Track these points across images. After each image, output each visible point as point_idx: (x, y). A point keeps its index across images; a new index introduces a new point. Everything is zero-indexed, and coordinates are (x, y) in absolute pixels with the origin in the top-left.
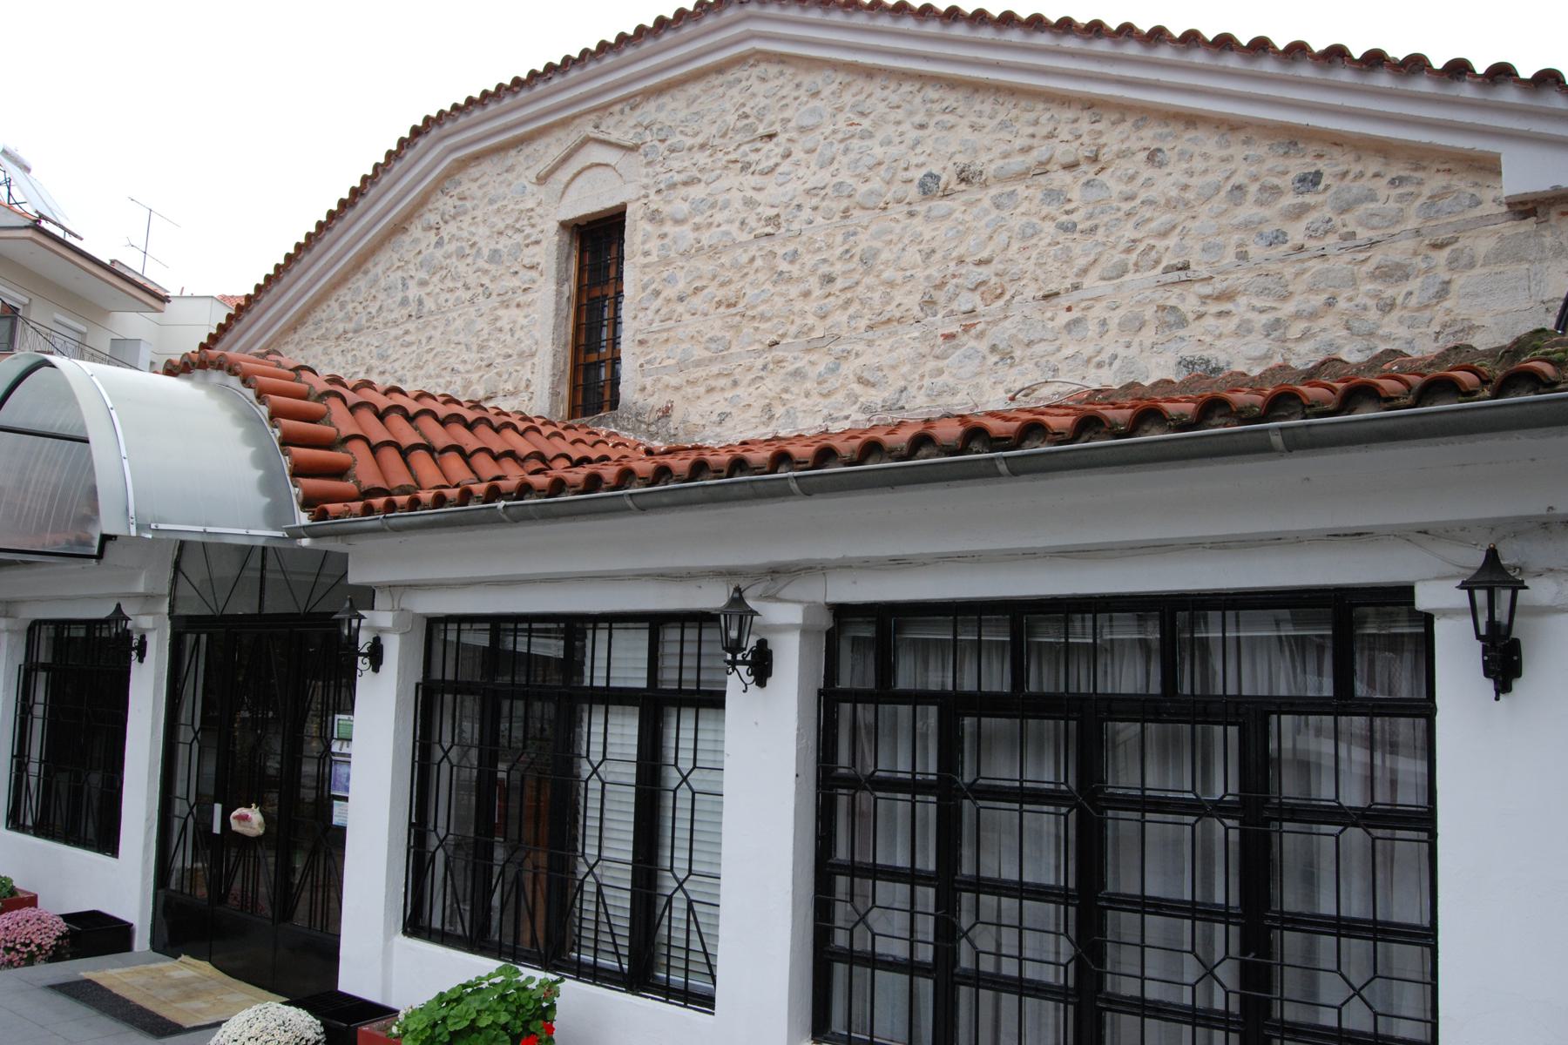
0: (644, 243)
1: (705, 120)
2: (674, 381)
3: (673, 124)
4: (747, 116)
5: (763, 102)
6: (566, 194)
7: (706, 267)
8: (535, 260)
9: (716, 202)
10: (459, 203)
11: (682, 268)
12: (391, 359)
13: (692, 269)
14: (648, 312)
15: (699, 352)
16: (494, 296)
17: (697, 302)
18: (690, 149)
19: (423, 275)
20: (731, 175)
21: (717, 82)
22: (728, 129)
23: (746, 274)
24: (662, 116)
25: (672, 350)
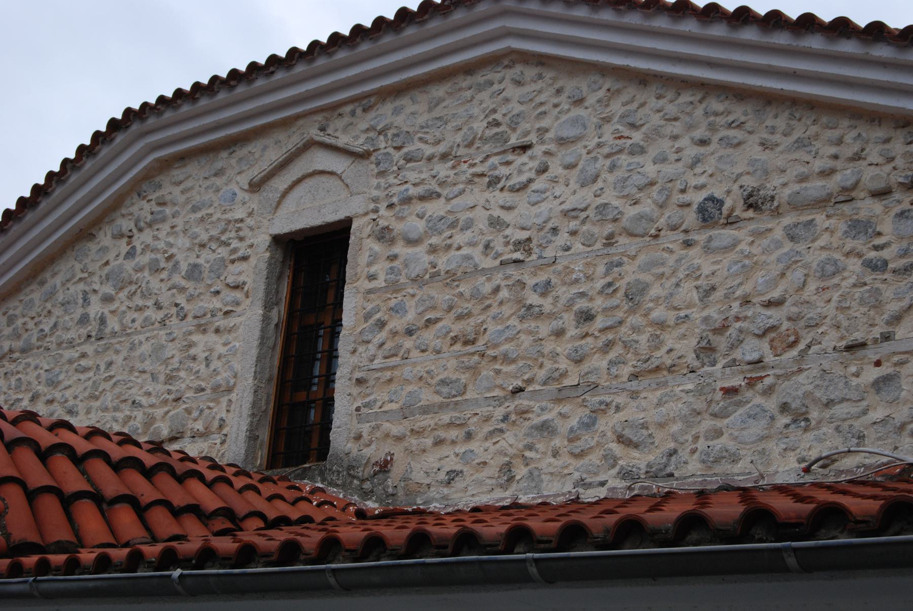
0: (369, 264)
4: (497, 124)
5: (517, 108)
6: (281, 206)
7: (442, 296)
8: (242, 279)
10: (157, 209)
11: (413, 296)
12: (62, 386)
13: (425, 297)
14: (370, 346)
15: (427, 397)
16: (189, 318)
17: (428, 336)
18: (430, 159)
20: (476, 190)
21: (464, 84)
22: (474, 138)
23: (489, 306)
24: (399, 120)
25: (395, 392)
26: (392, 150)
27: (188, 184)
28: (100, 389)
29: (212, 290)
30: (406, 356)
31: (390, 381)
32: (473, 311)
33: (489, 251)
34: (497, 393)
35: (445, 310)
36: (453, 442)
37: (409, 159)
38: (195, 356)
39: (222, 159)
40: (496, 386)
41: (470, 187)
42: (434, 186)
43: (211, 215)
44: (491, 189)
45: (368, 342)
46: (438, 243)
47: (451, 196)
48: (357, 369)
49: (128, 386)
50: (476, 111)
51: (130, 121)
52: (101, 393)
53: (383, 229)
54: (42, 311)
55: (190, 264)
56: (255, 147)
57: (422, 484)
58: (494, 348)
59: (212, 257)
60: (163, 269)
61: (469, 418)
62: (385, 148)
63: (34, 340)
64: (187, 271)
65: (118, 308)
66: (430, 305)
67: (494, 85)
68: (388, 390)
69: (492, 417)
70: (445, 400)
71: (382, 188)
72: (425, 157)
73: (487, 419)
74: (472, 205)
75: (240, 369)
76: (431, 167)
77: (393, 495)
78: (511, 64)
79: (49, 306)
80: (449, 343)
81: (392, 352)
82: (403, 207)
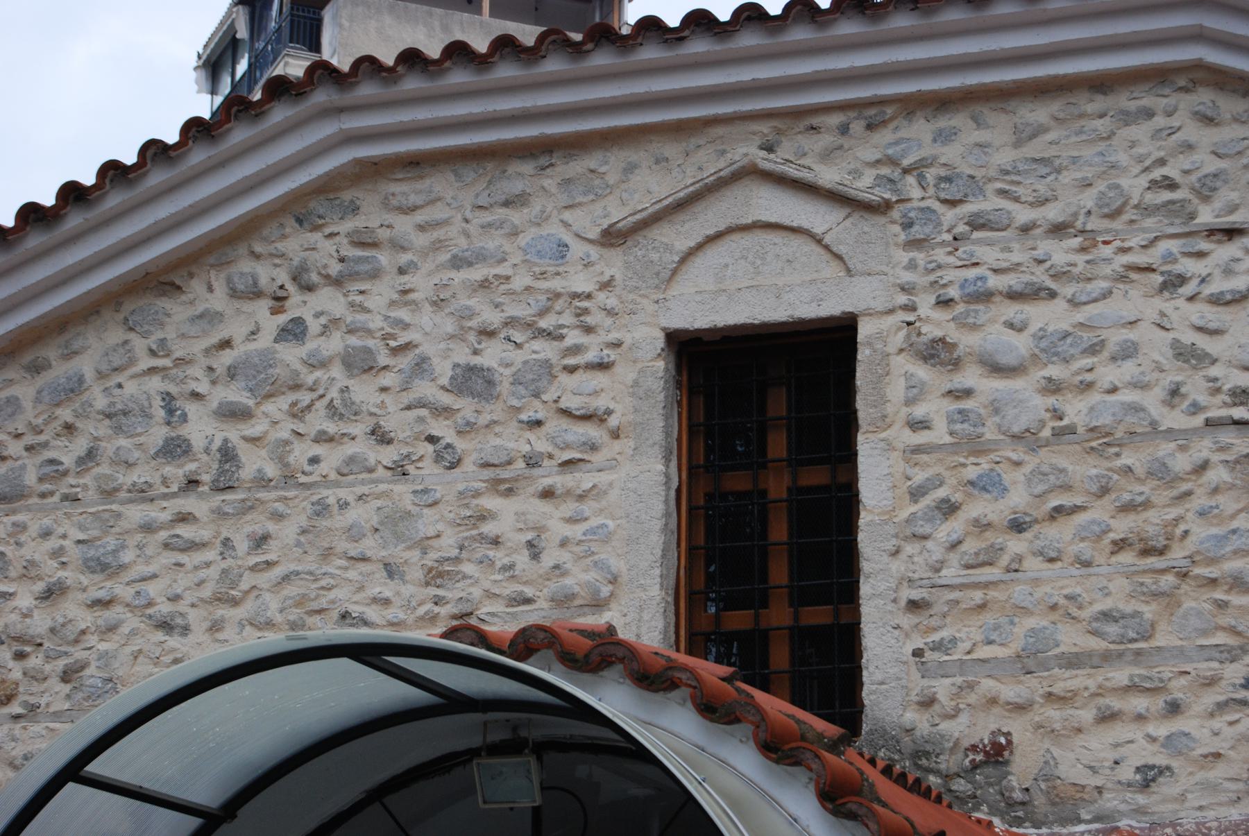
0: (909, 402)
1: (1066, 178)
2: (1009, 692)
3: (979, 174)
4: (1172, 186)
5: (1213, 165)
6: (678, 278)
7: (1084, 470)
8: (601, 403)
9: (1102, 343)
10: (352, 252)
11: (1018, 464)
12: (134, 573)
13: (1045, 468)
14: (929, 544)
15: (1071, 638)
16: (468, 466)
17: (1060, 534)
18: (1026, 229)
19: (235, 394)
20: (1133, 293)
21: (1090, 108)
22: (1125, 204)
23: (1188, 494)
24: (950, 153)
25: (996, 627)
26: (938, 203)
27: (437, 212)
28: (244, 586)
29: (524, 417)
30: (1015, 566)
31: (982, 607)
32: (1153, 499)
33: (1176, 400)
34: (1220, 638)
35: (1094, 494)
36: (1140, 718)
37: (977, 223)
38: (498, 537)
39: (520, 176)
40: (1220, 628)
41: (1121, 286)
42: (1040, 276)
43: (508, 278)
44: (1166, 294)
45: (925, 538)
46: (1062, 376)
47: (1084, 298)
48: (905, 584)
49: (323, 583)
50: (1122, 158)
51: (314, 84)
52: (247, 592)
53: (934, 341)
54: (46, 423)
55: (456, 365)
56: (606, 163)
57: (1084, 787)
58: (1208, 565)
59: (518, 357)
60: (385, 368)
61: (1170, 679)
62: (923, 198)
63: (30, 478)
64: (452, 378)
65: (266, 433)
66: (1058, 483)
67: (1156, 119)
68: (980, 623)
69: (1221, 678)
70: (1112, 647)
71: (921, 269)
72: (1013, 226)
73: (1211, 682)
74: (1133, 319)
75: (624, 568)
76: (1030, 243)
77: (1023, 803)
78: (1190, 85)
79: (65, 414)
80: (1108, 550)
81: (981, 558)
82: (972, 307)
